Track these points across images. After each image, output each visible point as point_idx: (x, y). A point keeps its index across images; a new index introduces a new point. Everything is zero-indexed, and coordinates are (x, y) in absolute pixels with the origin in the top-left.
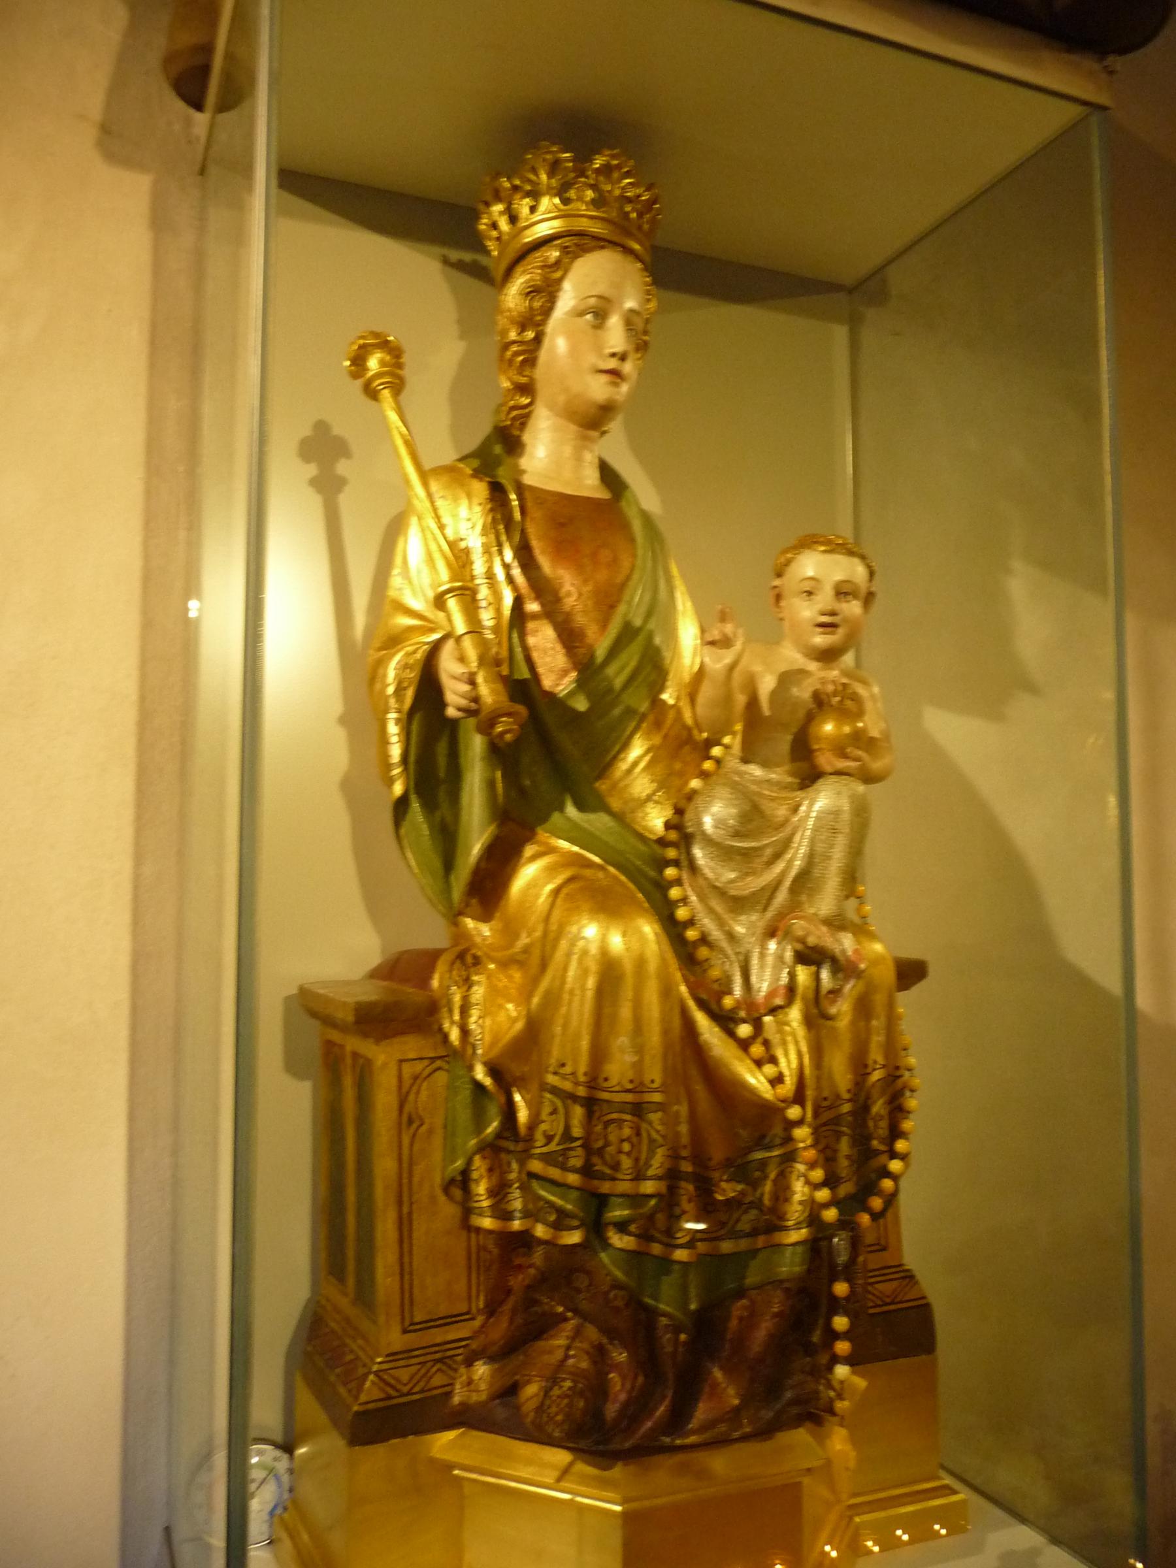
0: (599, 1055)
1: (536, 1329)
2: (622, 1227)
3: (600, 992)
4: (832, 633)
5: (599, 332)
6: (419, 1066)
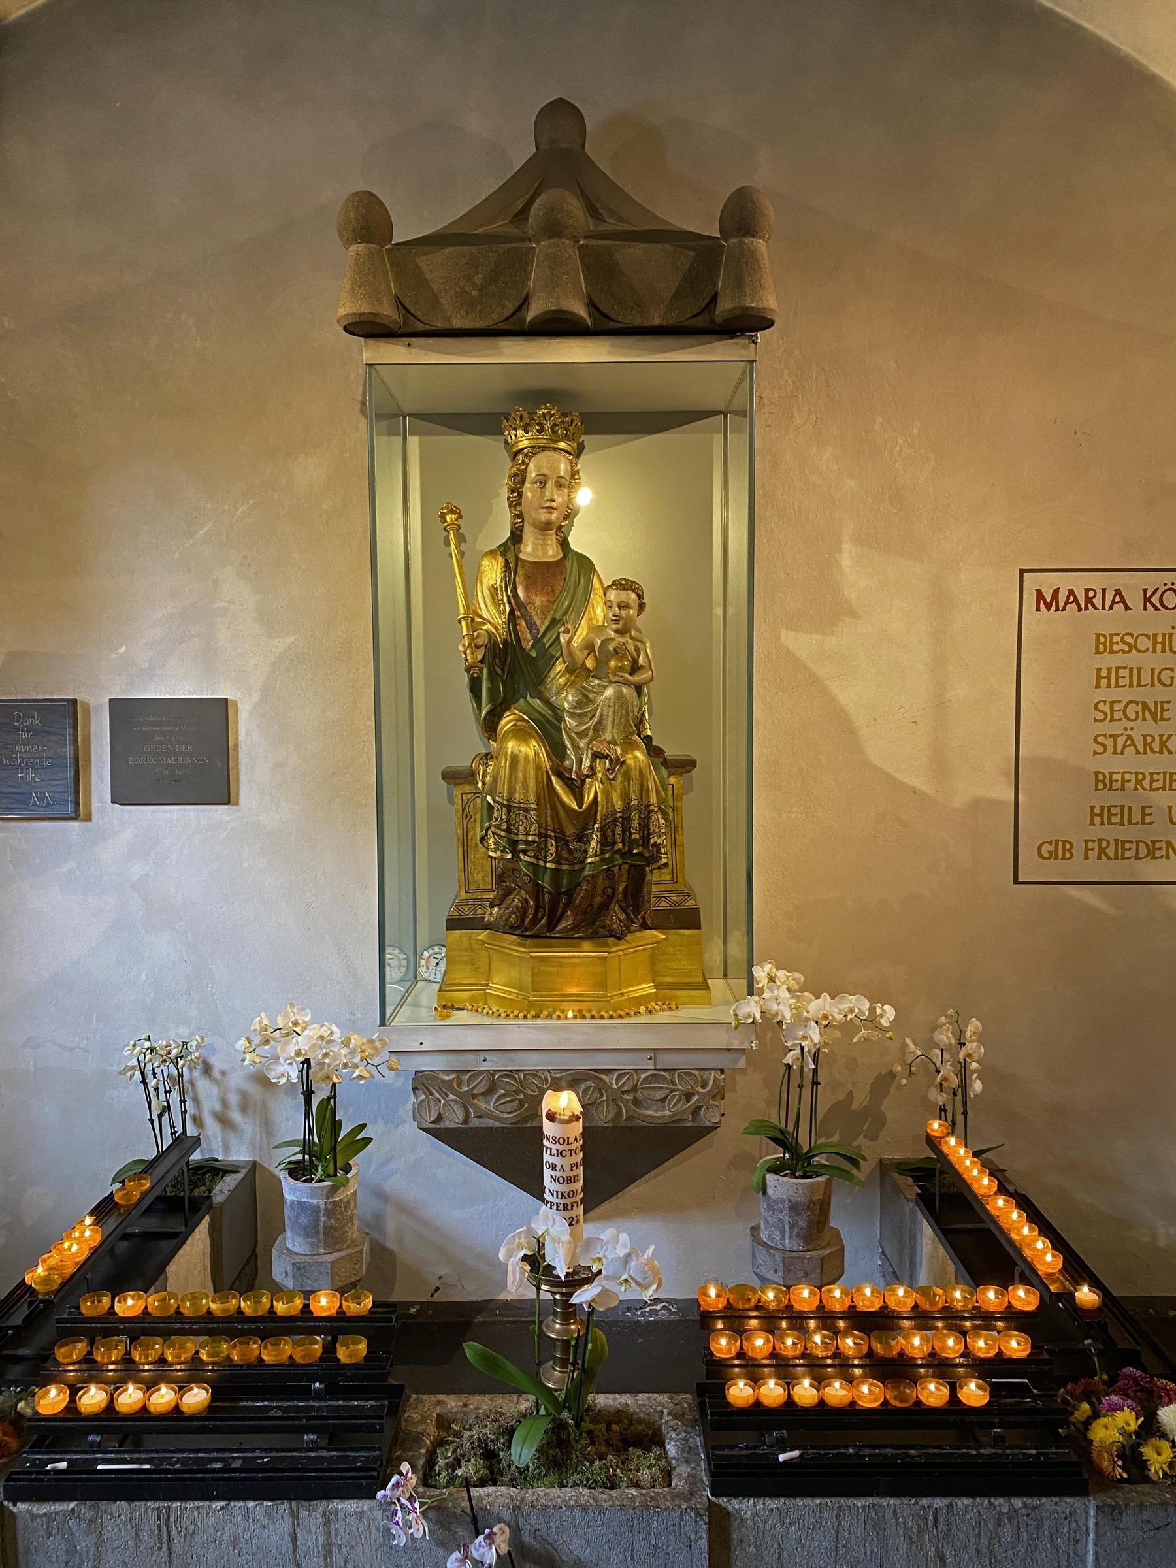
0: (512, 791)
1: (508, 892)
2: (524, 852)
3: (511, 767)
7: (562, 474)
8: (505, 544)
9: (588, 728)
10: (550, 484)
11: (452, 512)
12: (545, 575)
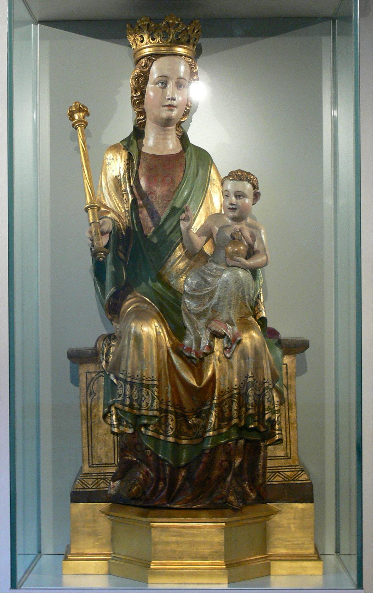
4: (235, 212)
5: (164, 90)
6: (94, 375)
11: (80, 110)
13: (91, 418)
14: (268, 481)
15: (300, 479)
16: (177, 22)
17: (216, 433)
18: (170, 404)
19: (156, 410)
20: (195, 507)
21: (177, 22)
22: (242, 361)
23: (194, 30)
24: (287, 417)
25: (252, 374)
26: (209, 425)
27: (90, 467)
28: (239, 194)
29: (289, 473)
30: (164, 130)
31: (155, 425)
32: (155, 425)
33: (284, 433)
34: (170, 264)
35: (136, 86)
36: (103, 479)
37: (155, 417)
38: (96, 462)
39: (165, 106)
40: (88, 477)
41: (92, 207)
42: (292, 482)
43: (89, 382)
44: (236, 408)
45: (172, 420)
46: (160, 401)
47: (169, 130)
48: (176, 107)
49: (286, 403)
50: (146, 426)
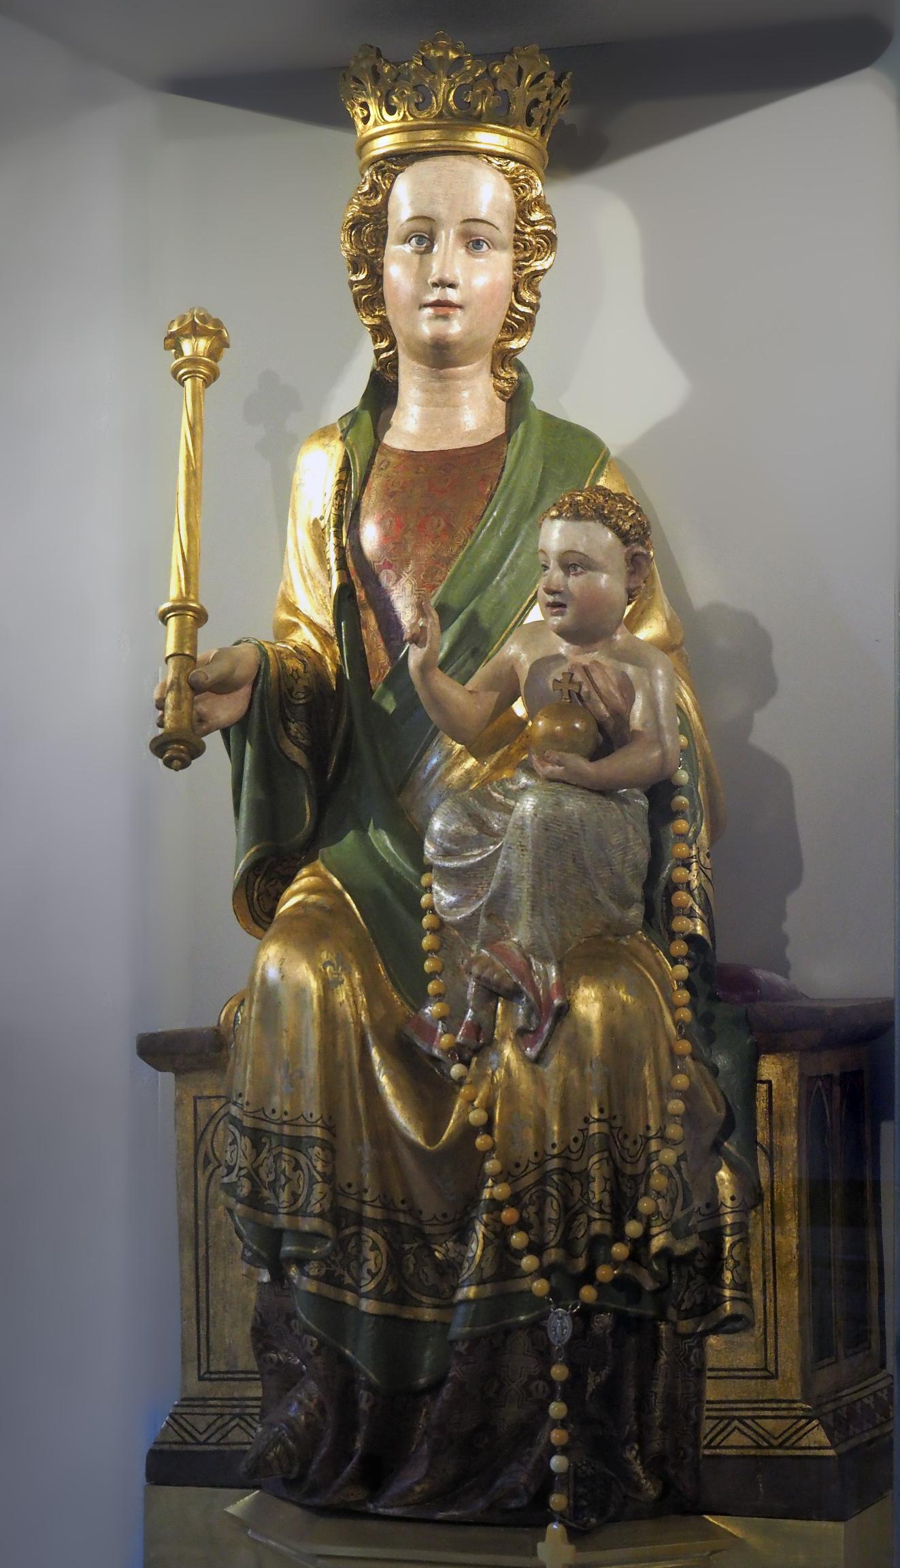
4: (562, 614)
5: (426, 257)
7: (483, 213)
8: (354, 416)
9: (475, 915)
10: (447, 239)
11: (195, 331)
12: (447, 487)
13: (207, 1232)
14: (708, 1446)
15: (804, 1443)
16: (452, 55)
17: (488, 1290)
18: (367, 1197)
19: (321, 1215)
20: (441, 1515)
21: (452, 55)
22: (574, 1072)
23: (520, 74)
24: (769, 1246)
25: (601, 1111)
26: (466, 1265)
27: (201, 1379)
28: (572, 559)
29: (769, 1424)
30: (441, 378)
31: (323, 1260)
32: (323, 1260)
33: (756, 1294)
34: (424, 776)
35: (353, 252)
36: (240, 1416)
37: (317, 1235)
38: (219, 1365)
39: (426, 306)
40: (197, 1410)
41: (179, 609)
42: (780, 1452)
43: (200, 1128)
44: (554, 1216)
45: (375, 1247)
46: (333, 1190)
47: (455, 377)
48: (460, 307)
49: (767, 1204)
50: (301, 1262)
